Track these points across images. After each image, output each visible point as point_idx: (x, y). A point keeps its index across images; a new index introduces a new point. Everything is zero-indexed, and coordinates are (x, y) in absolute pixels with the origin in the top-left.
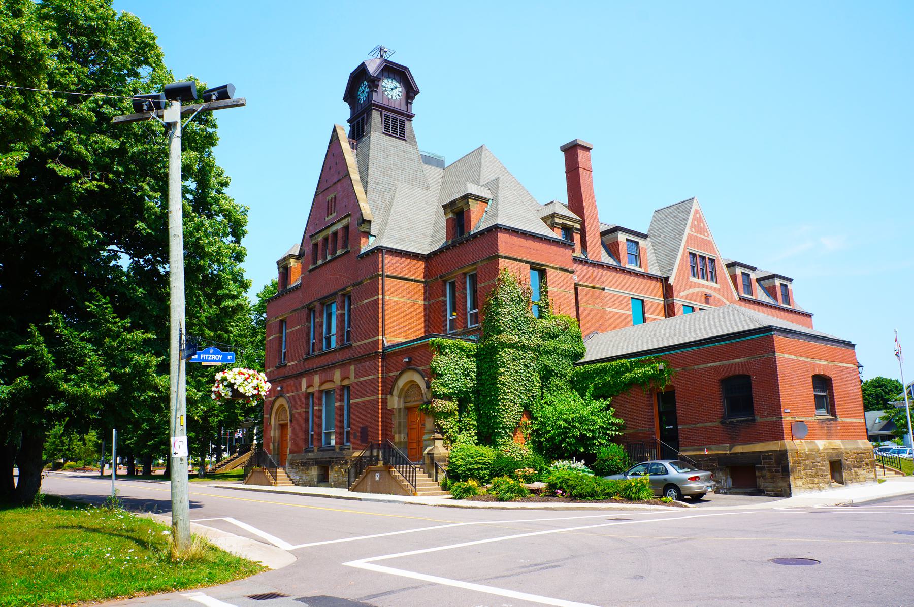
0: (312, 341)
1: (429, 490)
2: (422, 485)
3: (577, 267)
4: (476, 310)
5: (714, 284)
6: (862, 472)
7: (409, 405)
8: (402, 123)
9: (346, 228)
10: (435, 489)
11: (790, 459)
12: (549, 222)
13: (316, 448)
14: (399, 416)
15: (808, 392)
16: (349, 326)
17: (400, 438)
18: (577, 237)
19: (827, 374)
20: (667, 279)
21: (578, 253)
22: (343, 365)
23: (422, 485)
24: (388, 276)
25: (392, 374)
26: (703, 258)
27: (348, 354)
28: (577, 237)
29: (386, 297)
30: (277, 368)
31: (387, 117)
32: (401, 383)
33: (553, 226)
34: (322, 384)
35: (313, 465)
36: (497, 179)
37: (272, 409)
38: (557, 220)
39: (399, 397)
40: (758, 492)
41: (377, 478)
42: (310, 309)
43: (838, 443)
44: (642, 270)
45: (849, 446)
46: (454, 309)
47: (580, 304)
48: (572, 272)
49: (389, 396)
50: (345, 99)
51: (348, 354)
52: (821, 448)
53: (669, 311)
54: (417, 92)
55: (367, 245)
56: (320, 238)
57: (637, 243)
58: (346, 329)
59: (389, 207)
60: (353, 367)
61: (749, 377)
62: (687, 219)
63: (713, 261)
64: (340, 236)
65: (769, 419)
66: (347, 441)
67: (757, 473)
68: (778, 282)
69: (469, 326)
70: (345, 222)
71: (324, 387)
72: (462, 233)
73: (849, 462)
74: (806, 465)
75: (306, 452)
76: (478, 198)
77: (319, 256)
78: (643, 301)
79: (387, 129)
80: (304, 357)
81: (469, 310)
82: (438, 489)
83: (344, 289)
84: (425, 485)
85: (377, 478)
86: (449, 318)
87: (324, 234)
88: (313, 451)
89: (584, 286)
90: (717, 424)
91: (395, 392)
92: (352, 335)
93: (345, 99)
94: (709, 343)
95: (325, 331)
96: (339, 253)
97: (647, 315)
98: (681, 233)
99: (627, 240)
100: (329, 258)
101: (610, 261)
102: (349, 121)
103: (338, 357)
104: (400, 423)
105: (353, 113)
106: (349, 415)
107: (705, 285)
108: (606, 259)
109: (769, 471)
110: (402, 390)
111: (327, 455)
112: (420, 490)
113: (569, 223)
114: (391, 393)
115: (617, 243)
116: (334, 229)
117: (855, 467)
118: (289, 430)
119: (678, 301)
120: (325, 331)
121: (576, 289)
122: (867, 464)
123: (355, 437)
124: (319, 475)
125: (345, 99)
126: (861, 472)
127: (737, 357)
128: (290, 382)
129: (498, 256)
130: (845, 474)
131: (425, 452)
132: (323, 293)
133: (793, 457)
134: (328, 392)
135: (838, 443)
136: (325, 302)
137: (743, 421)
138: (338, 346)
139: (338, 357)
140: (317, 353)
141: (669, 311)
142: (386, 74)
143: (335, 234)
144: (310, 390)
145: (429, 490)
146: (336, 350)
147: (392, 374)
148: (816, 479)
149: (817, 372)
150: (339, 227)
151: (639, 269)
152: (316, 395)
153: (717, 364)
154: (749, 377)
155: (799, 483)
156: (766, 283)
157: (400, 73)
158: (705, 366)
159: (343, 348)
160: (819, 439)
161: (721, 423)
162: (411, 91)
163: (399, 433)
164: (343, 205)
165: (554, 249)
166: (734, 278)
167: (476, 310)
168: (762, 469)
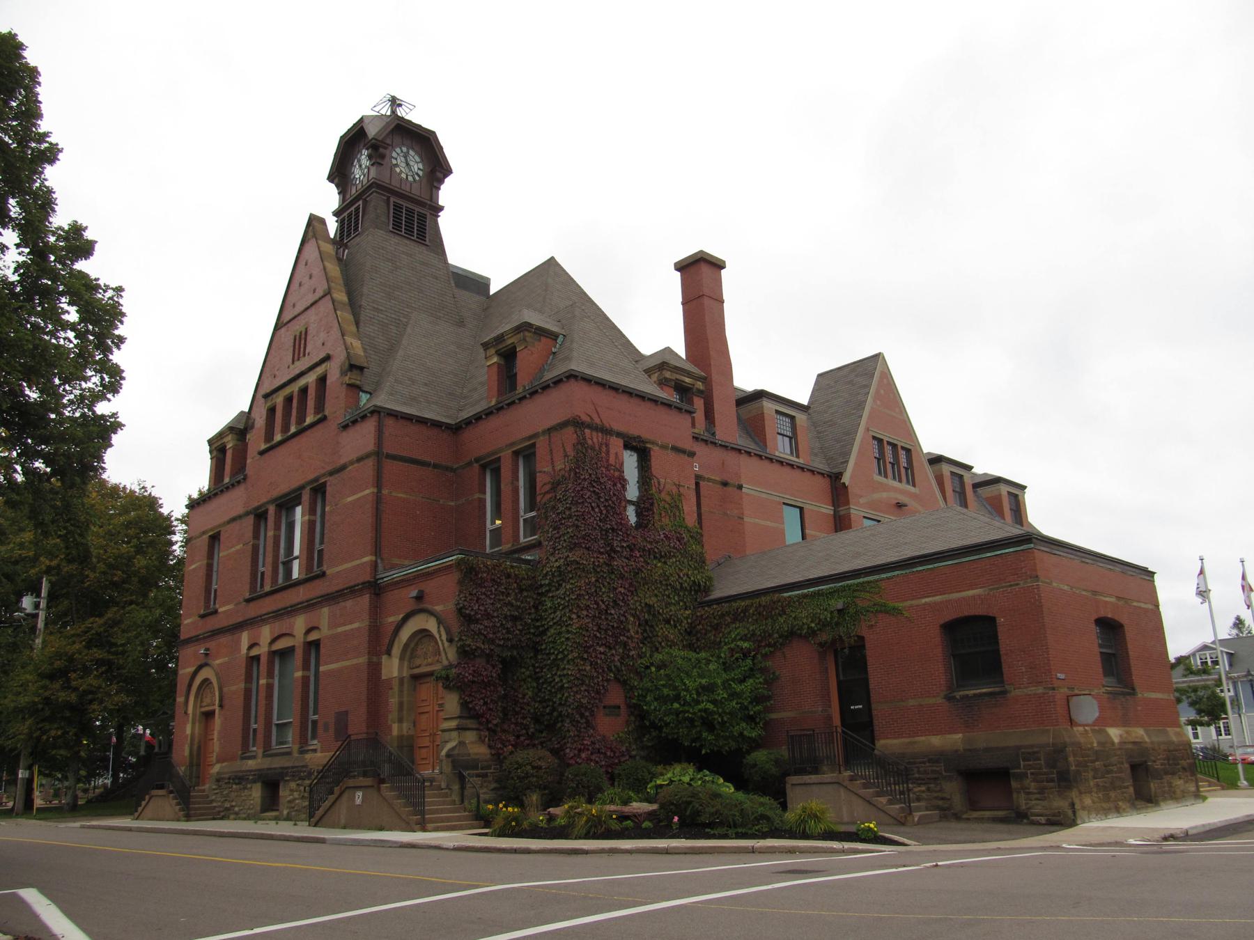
0: (261, 569)
1: (448, 820)
2: (436, 812)
3: (699, 449)
4: (533, 514)
5: (910, 488)
6: (1180, 782)
7: (416, 671)
8: (422, 218)
10: (459, 819)
12: (655, 377)
13: (260, 752)
14: (401, 691)
15: (1090, 643)
16: (322, 542)
17: (400, 729)
18: (699, 403)
19: (1116, 618)
20: (839, 476)
21: (701, 427)
22: (309, 606)
23: (436, 812)
24: (389, 456)
25: (391, 619)
26: (894, 446)
27: (319, 588)
28: (699, 403)
29: (385, 492)
30: (202, 616)
31: (398, 208)
32: (405, 634)
33: (662, 383)
35: (254, 781)
37: (190, 685)
39: (402, 659)
40: (1019, 819)
41: (358, 801)
42: (260, 516)
43: (1139, 733)
44: (801, 461)
45: (1155, 739)
46: (498, 513)
47: (704, 509)
48: (692, 454)
49: (384, 658)
50: (331, 178)
51: (319, 588)
52: (1116, 740)
53: (841, 523)
54: (447, 171)
56: (279, 399)
57: (792, 418)
58: (317, 547)
59: (392, 349)
60: (325, 611)
61: (991, 620)
62: (868, 386)
63: (908, 451)
65: (1032, 690)
66: (314, 737)
67: (1014, 784)
68: (1004, 489)
69: (522, 540)
70: (320, 370)
71: (280, 645)
72: (513, 387)
73: (1158, 766)
74: (1095, 770)
75: (243, 758)
76: (541, 332)
78: (801, 509)
79: (397, 225)
80: (247, 596)
81: (522, 513)
82: (465, 818)
83: (316, 480)
84: (442, 811)
85: (358, 801)
86: (489, 526)
87: (287, 391)
88: (254, 757)
89: (709, 480)
90: (940, 700)
91: (396, 651)
92: (326, 557)
94: (921, 564)
95: (282, 551)
96: (309, 420)
97: (807, 531)
98: (861, 405)
99: (777, 412)
100: (293, 429)
101: (751, 446)
102: (336, 214)
103: (301, 594)
104: (401, 704)
105: (343, 200)
106: (316, 692)
107: (897, 489)
108: (742, 441)
109: (1035, 780)
110: (406, 645)
111: (278, 763)
112: (432, 821)
113: (687, 380)
114: (389, 653)
115: (761, 417)
116: (302, 382)
117: (1166, 773)
118: (218, 720)
119: (856, 511)
120: (282, 551)
121: (697, 484)
122: (1184, 769)
123: (326, 728)
124: (263, 798)
125: (331, 178)
126: (1178, 783)
127: (971, 587)
128: (224, 640)
130: (1153, 786)
131: (443, 753)
132: (284, 488)
133: (1075, 755)
134: (285, 654)
135: (1139, 733)
136: (286, 504)
137: (985, 694)
138: (304, 576)
139: (301, 594)
140: (267, 588)
141: (841, 523)
142: (397, 139)
144: (254, 652)
145: (448, 820)
146: (299, 583)
147: (391, 619)
148: (1113, 794)
149: (1102, 614)
150: (295, 388)
151: (794, 459)
152: (264, 660)
153: (938, 598)
154: (991, 620)
155: (1088, 801)
156: (986, 492)
158: (914, 602)
159: (313, 576)
160: (1112, 726)
161: (949, 698)
162: (438, 168)
163: (400, 721)
164: (320, 342)
165: (662, 413)
166: (940, 480)
167: (533, 514)
168: (1022, 776)
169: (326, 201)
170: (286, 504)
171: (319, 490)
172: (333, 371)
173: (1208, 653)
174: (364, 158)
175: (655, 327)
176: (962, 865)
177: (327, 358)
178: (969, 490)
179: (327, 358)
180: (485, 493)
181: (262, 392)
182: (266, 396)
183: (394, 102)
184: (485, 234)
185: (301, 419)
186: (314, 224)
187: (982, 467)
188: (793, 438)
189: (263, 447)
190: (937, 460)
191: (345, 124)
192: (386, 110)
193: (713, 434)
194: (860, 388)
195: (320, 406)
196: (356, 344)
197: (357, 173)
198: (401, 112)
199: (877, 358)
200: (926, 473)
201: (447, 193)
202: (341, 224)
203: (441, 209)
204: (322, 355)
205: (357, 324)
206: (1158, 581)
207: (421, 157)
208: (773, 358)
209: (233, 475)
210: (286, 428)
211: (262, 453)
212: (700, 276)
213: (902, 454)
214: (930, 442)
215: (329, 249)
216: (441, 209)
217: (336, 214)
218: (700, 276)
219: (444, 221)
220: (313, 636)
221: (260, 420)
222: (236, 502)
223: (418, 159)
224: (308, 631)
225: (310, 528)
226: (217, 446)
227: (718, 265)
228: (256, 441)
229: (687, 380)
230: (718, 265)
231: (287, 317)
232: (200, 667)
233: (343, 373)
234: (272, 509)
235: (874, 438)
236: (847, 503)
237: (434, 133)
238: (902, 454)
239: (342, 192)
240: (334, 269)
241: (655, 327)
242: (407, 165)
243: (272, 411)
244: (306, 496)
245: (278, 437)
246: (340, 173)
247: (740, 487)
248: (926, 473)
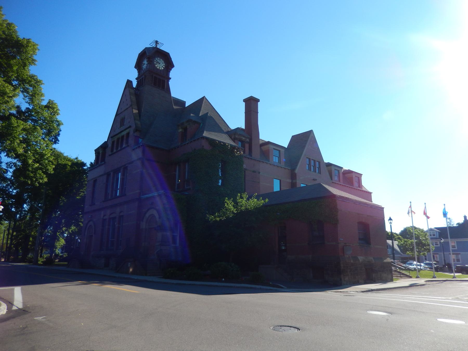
8: (164, 82)
9: (128, 134)
11: (342, 265)
18: (247, 146)
26: (314, 161)
28: (247, 146)
34: (111, 214)
36: (208, 113)
38: (237, 136)
42: (108, 174)
55: (42, 98)
56: (115, 139)
57: (279, 151)
64: (125, 137)
70: (127, 131)
71: (112, 216)
77: (115, 148)
86: (177, 183)
93: (135, 67)
99: (274, 149)
102: (136, 79)
105: (139, 74)
120: (115, 187)
129: (392, 240)
136: (116, 171)
143: (123, 136)
144: (105, 218)
146: (119, 197)
150: (124, 133)
157: (166, 57)
159: (123, 194)
162: (169, 65)
169: (133, 75)
170: (116, 171)
171: (125, 168)
172: (131, 130)
173: (431, 232)
174: (145, 62)
175: (235, 119)
176: (442, 306)
177: (130, 127)
178: (341, 175)
179: (130, 127)
180: (176, 172)
181: (111, 136)
182: (112, 137)
183: (157, 42)
184: (184, 88)
185: (122, 145)
186: (129, 83)
187: (346, 168)
188: (279, 157)
189: (110, 153)
190: (329, 165)
191: (140, 49)
192: (154, 45)
193: (251, 156)
194: (304, 142)
195: (127, 142)
196: (139, 123)
197: (144, 67)
198: (158, 47)
199: (311, 132)
200: (324, 170)
201: (172, 74)
202: (138, 82)
203: (170, 78)
204: (129, 126)
205: (140, 117)
206: (385, 210)
207: (164, 61)
208: (276, 131)
209: (101, 162)
210: (117, 148)
211: (110, 155)
212: (251, 105)
213: (317, 163)
214: (327, 159)
215: (132, 91)
216: (170, 78)
217: (136, 79)
218: (251, 105)
219: (171, 83)
220: (122, 214)
221: (110, 145)
222: (100, 170)
223: (163, 62)
224: (121, 212)
225: (123, 180)
226: (97, 151)
227: (257, 101)
228: (108, 151)
229: (243, 138)
230: (257, 101)
231: (119, 113)
232: (89, 221)
233: (134, 132)
234: (112, 173)
235: (307, 158)
236: (296, 179)
237: (169, 53)
238: (317, 163)
239: (139, 72)
240: (134, 98)
241: (235, 119)
242: (160, 65)
243: (113, 143)
244: (122, 170)
245: (115, 151)
246: (138, 66)
247: (259, 173)
248: (324, 170)
